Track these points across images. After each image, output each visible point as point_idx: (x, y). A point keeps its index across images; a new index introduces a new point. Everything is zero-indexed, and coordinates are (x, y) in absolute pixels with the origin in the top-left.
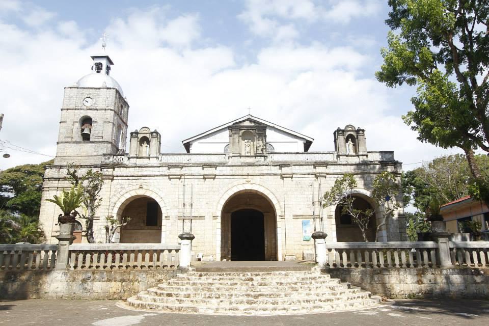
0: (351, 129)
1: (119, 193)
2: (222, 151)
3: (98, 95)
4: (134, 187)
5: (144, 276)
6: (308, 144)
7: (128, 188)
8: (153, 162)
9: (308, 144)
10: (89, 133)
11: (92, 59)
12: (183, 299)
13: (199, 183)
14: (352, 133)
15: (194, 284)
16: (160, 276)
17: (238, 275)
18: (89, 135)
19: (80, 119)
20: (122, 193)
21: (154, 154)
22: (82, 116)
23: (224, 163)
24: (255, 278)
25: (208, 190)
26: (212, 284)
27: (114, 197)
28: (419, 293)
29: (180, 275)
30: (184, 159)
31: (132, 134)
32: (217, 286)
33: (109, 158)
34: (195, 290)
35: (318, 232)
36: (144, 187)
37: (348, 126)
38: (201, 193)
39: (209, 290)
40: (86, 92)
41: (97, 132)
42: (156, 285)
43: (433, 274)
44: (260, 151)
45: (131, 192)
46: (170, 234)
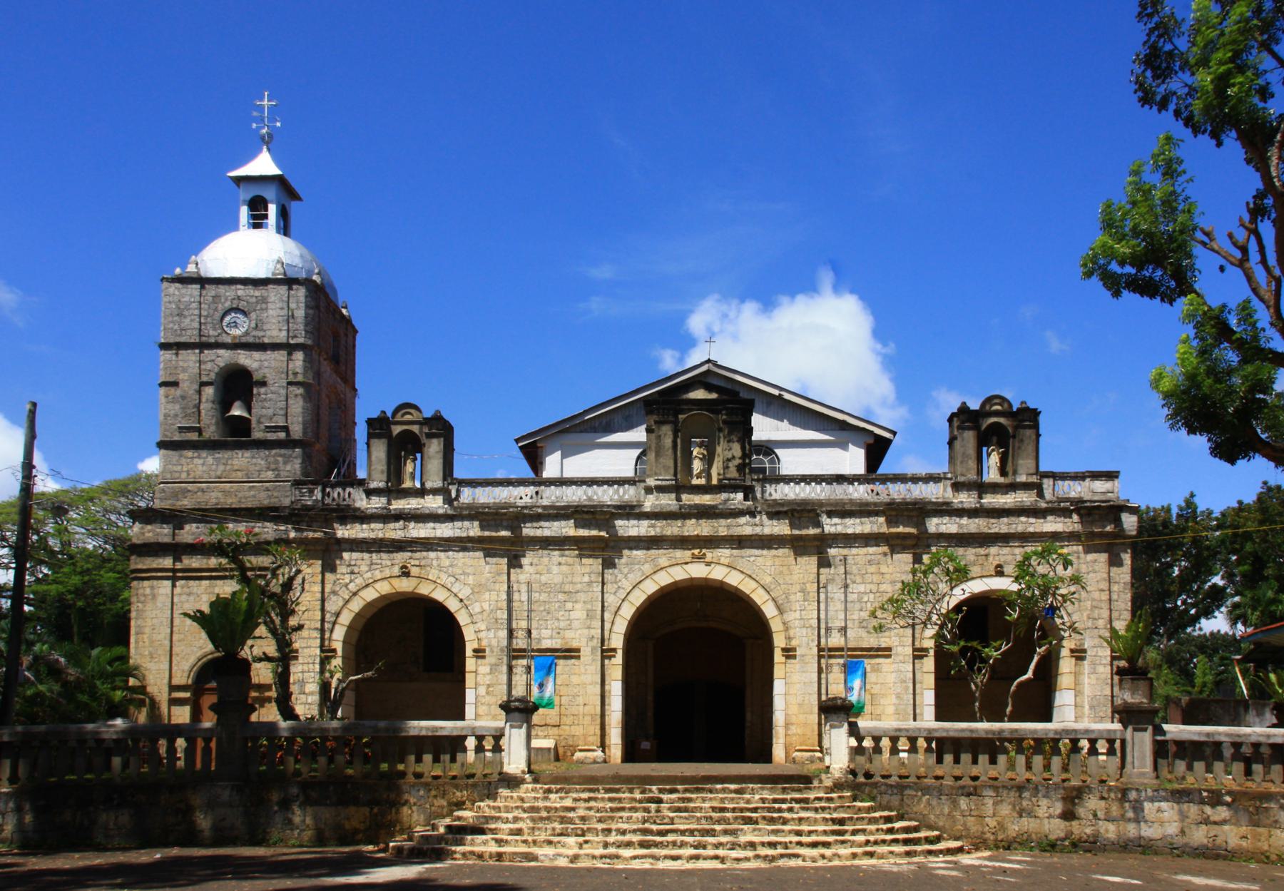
0: (999, 407)
1: (346, 585)
2: (629, 472)
3: (264, 300)
4: (387, 573)
5: (422, 793)
6: (877, 449)
7: (369, 575)
8: (434, 503)
9: (877, 449)
10: (245, 415)
11: (234, 185)
12: (505, 837)
13: (563, 560)
14: (1002, 420)
15: (534, 809)
16: (458, 794)
17: (631, 791)
18: (248, 421)
19: (217, 374)
20: (352, 587)
21: (435, 481)
22: (222, 364)
23: (632, 507)
24: (665, 797)
25: (586, 579)
26: (573, 809)
27: (334, 598)
28: (1063, 839)
29: (504, 792)
30: (522, 496)
31: (370, 422)
32: (581, 812)
33: (311, 492)
34: (533, 820)
35: (835, 699)
36: (414, 571)
37: (989, 400)
38: (567, 588)
39: (563, 820)
40: (229, 292)
41: (270, 412)
42: (450, 814)
43: (1102, 798)
44: (732, 473)
45: (378, 586)
46: (488, 693)
